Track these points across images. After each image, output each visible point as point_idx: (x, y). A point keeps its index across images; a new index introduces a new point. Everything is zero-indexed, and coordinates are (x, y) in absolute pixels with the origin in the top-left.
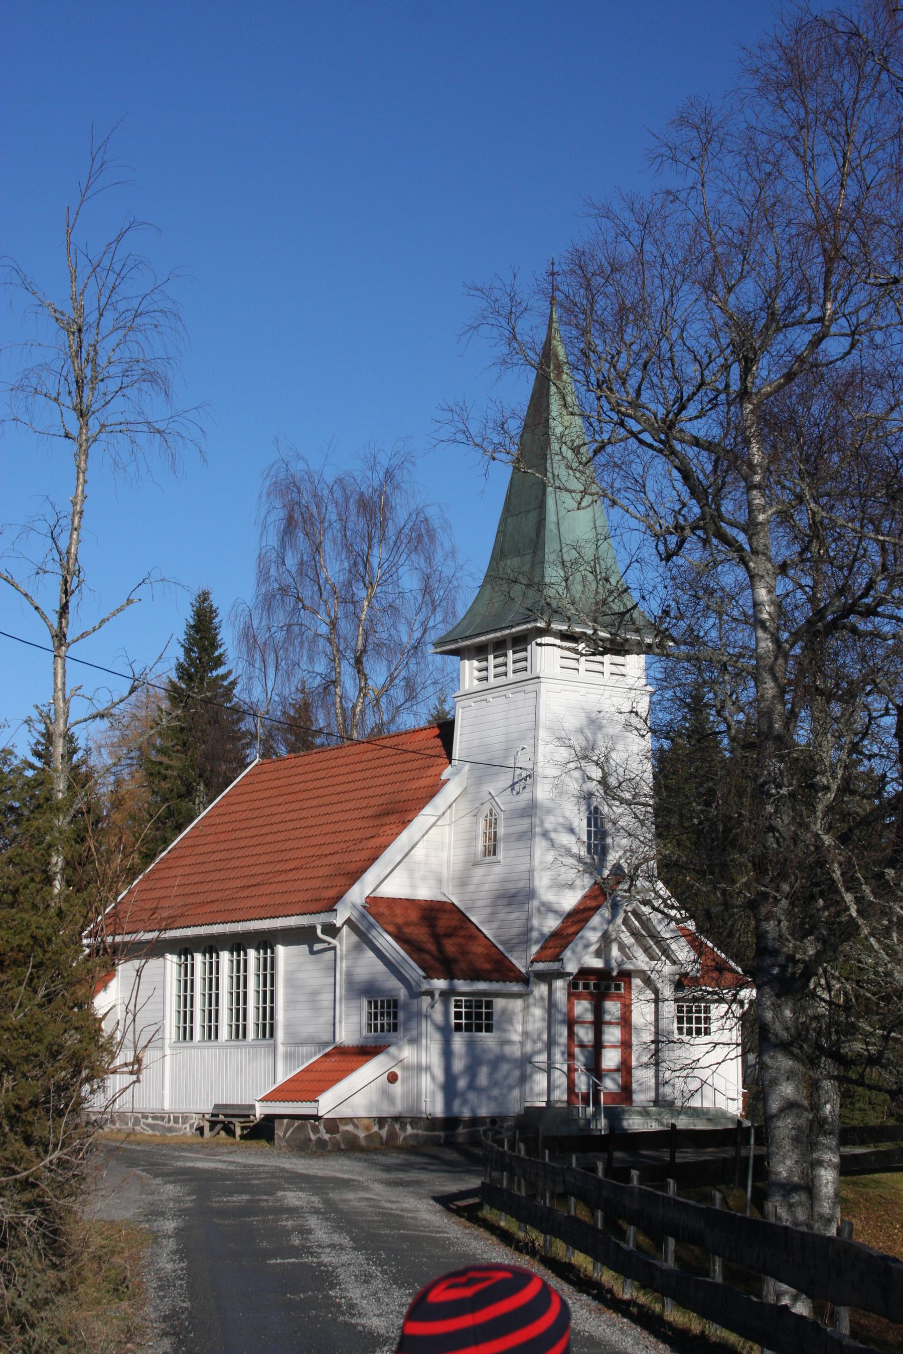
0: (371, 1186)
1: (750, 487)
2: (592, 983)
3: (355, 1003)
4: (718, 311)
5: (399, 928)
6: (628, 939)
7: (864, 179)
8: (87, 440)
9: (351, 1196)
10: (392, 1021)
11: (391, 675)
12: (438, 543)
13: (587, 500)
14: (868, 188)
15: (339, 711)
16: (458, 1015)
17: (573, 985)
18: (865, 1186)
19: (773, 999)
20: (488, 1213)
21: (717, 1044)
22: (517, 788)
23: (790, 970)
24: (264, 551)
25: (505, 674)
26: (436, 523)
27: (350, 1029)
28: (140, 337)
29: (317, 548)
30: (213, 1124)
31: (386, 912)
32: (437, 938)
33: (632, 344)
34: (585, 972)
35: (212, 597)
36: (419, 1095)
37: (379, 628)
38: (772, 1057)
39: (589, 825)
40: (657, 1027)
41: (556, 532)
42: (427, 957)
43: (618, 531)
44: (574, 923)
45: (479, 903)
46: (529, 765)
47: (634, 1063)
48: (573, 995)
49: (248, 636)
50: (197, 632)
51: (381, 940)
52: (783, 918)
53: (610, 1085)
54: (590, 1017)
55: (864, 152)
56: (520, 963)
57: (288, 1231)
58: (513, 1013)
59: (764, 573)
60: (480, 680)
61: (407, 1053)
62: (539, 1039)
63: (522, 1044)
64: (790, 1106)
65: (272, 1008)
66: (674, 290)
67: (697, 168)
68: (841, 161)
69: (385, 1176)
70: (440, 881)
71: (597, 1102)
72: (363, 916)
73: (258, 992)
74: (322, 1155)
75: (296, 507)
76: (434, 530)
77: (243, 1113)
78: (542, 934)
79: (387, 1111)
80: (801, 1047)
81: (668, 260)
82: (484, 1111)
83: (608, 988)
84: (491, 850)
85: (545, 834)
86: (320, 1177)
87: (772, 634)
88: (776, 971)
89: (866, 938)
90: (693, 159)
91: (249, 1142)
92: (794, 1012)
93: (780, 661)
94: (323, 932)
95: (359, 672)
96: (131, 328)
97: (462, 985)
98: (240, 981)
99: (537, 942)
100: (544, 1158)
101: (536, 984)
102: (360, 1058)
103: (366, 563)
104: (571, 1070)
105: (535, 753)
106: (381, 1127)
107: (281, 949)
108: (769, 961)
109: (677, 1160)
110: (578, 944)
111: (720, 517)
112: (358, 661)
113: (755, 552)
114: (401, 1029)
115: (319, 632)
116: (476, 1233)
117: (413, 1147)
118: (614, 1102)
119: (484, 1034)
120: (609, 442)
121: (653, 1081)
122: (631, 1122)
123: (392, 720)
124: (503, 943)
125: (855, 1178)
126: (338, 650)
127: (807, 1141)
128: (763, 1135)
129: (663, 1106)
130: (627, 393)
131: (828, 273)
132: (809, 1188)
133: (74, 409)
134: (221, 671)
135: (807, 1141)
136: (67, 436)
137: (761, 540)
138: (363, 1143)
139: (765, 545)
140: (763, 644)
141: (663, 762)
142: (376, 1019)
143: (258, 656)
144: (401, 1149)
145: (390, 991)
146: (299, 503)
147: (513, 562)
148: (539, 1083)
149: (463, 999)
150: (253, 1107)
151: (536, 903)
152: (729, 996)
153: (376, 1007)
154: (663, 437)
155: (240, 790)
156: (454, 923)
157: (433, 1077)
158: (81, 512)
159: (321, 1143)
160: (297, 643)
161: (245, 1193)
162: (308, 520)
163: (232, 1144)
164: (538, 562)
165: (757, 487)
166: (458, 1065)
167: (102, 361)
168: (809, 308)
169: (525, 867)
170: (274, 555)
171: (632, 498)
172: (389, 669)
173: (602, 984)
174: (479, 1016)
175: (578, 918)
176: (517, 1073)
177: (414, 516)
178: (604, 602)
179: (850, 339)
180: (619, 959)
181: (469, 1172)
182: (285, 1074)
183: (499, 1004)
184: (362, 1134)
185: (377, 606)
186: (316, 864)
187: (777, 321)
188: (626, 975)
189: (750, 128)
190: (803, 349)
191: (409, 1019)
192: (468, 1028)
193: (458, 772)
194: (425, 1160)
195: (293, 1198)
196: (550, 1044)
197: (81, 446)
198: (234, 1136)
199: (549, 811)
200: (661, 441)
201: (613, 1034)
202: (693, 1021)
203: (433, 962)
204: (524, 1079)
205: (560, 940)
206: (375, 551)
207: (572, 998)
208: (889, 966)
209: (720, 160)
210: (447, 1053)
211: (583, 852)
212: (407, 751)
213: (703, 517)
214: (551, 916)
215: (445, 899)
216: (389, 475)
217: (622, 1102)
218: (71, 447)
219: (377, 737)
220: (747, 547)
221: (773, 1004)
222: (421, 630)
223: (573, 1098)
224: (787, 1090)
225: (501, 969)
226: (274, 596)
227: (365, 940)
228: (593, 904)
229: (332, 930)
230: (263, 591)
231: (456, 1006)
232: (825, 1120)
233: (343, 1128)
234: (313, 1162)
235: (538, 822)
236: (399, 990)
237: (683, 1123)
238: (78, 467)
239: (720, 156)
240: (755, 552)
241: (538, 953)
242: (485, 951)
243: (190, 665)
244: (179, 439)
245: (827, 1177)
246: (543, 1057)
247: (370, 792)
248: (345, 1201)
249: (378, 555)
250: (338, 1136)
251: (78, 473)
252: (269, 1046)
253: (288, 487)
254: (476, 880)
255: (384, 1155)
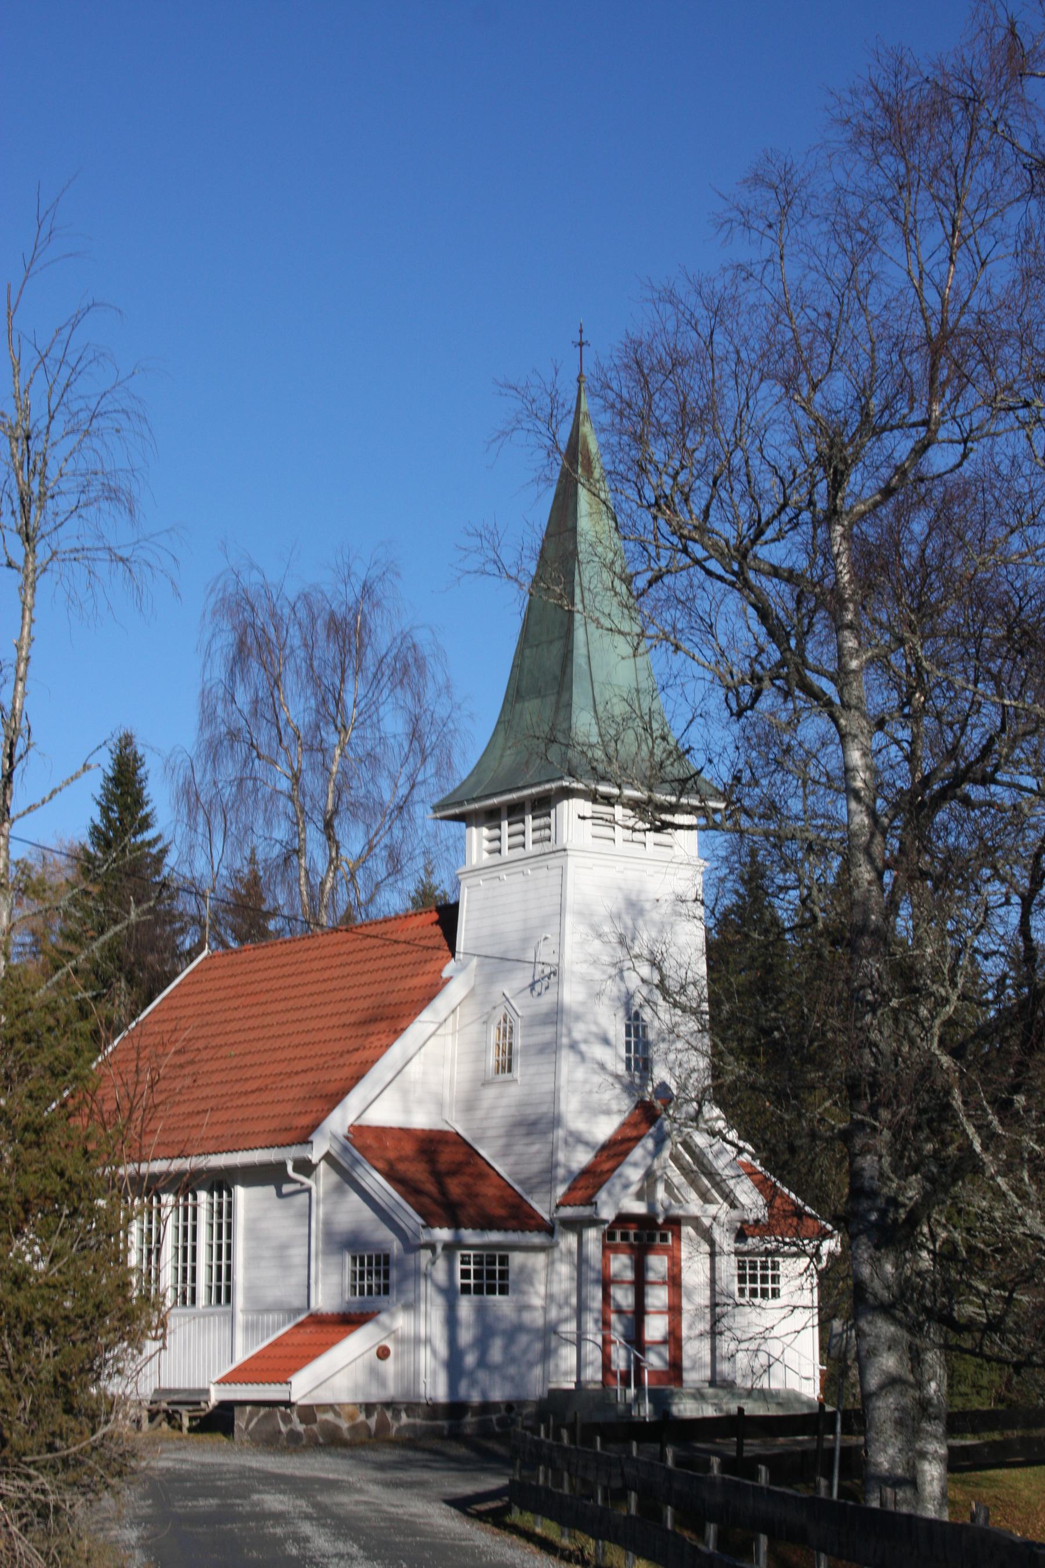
0: (366, 1487)
1: (840, 627)
2: (632, 1232)
3: (335, 1259)
4: (801, 412)
5: (391, 1164)
6: (676, 1176)
7: (978, 253)
8: (34, 571)
9: (343, 1499)
10: (382, 1281)
11: (370, 842)
12: (429, 675)
13: (645, 644)
14: (983, 264)
15: (303, 888)
16: (465, 1274)
17: (609, 1235)
18: (977, 1485)
19: (872, 1250)
20: (516, 1517)
21: (795, 1307)
22: (538, 987)
23: (891, 1216)
24: (208, 686)
25: (523, 845)
26: (426, 650)
27: (329, 1292)
28: (96, 443)
29: (276, 682)
30: (152, 1416)
31: (375, 1145)
32: (439, 1177)
33: (694, 451)
34: (623, 1219)
35: (136, 741)
36: (416, 1374)
37: (354, 783)
38: (870, 1323)
39: (628, 1034)
40: (713, 1290)
41: (586, 667)
42: (426, 1201)
43: (678, 681)
44: (609, 1158)
45: (490, 1133)
46: (554, 960)
47: (685, 1332)
48: (608, 1247)
49: (189, 796)
50: (117, 786)
51: (369, 1180)
52: (884, 1152)
53: (654, 1361)
54: (629, 1275)
55: (978, 218)
56: (542, 1207)
57: (280, 1539)
58: (534, 1271)
59: (858, 732)
60: (491, 852)
61: (402, 1322)
62: (567, 1302)
63: (545, 1309)
64: (892, 1382)
65: (229, 1267)
66: (750, 391)
67: (774, 236)
68: (950, 231)
69: (379, 1475)
70: (440, 1105)
71: (639, 1383)
72: (345, 1149)
73: (211, 1246)
74: (295, 1451)
75: (249, 630)
76: (424, 658)
77: (193, 1399)
78: (570, 1172)
79: (376, 1395)
80: (905, 1310)
81: (743, 355)
82: (497, 1395)
83: (652, 1238)
84: (506, 1066)
85: (573, 1046)
86: (301, 1478)
87: (868, 807)
88: (874, 1217)
89: (992, 1178)
90: (770, 226)
91: (200, 1437)
92: (896, 1266)
93: (878, 839)
94: (295, 1170)
95: (329, 838)
96: (87, 433)
97: (470, 1236)
98: (188, 1233)
99: (563, 1181)
100: (595, 1447)
101: (562, 1234)
102: (342, 1329)
103: (338, 701)
104: (607, 1342)
105: (560, 944)
106: (369, 1415)
107: (240, 1192)
108: (865, 1204)
109: (745, 1454)
110: (615, 1183)
111: (805, 663)
112: (328, 825)
113: (846, 706)
114: (393, 1292)
115: (278, 788)
116: (509, 1541)
117: (409, 1440)
118: (659, 1382)
119: (497, 1297)
120: (669, 572)
121: (707, 1358)
122: (682, 1407)
123: (371, 900)
124: (521, 1182)
125: (965, 1475)
126: (302, 811)
127: (910, 1423)
128: (857, 1419)
129: (722, 1387)
130: (690, 512)
131: (934, 367)
132: (912, 1482)
133: (19, 533)
134: (149, 835)
135: (910, 1423)
136: (10, 565)
137: (856, 690)
138: (347, 1435)
139: (859, 698)
140: (857, 819)
141: (716, 952)
142: (362, 1278)
143: (201, 818)
144: (394, 1443)
145: (380, 1243)
146: (253, 625)
147: (530, 707)
148: (566, 1358)
149: (472, 1253)
150: (207, 1391)
151: (561, 1133)
152: (810, 1249)
153: (362, 1264)
154: (736, 567)
155: (184, 990)
156: (460, 1157)
157: (434, 1352)
158: (28, 659)
159: (294, 1436)
160: (250, 801)
161: (213, 1497)
162: (264, 645)
163: (180, 1439)
164: (564, 706)
165: (850, 626)
166: (466, 1336)
167: (52, 472)
168: (911, 409)
169: (549, 1087)
170: (221, 692)
171: (696, 639)
172: (367, 833)
173: (645, 1234)
174: (491, 1274)
175: (615, 1150)
176: (538, 1346)
177: (399, 641)
178: (661, 765)
179: (960, 448)
180: (666, 1203)
181: (483, 1470)
182: (246, 1349)
183: (517, 1259)
184: (345, 1425)
185: (351, 755)
186: (284, 1084)
187: (872, 428)
188: (675, 1223)
189: (839, 188)
190: (904, 458)
191: (403, 1278)
192: (478, 1290)
193: (463, 968)
194: (426, 1456)
195: (274, 1501)
196: (581, 1309)
197: (27, 577)
198: (180, 1428)
199: (578, 1018)
200: (734, 573)
201: (658, 1297)
202: (758, 1280)
203: (435, 1208)
204: (547, 1354)
205: (591, 1180)
206: (349, 685)
207: (607, 1252)
208: (1020, 1210)
209: (802, 226)
210: (452, 1322)
211: (621, 1068)
212: (396, 942)
213: (782, 663)
214: (580, 1148)
215: (446, 1128)
216: (367, 590)
217: (669, 1382)
218: (16, 578)
219: (347, 923)
220: (837, 701)
221: (871, 1257)
222: (407, 787)
223: (610, 1378)
224: (889, 1362)
225: (517, 1215)
226: (221, 742)
227: (348, 1179)
228: (631, 1133)
229: (306, 1167)
230: (207, 735)
231: (463, 1263)
232: (929, 1402)
233: (321, 1417)
234: (285, 1459)
235: (564, 1031)
236: (392, 1242)
237: (753, 1408)
238: (24, 603)
239: (803, 222)
240: (846, 706)
241: (565, 1195)
242: (498, 1193)
243: (108, 828)
244: (145, 568)
245: (932, 1472)
246: (571, 1327)
247: (352, 993)
248: (338, 1505)
249: (353, 691)
250: (315, 1427)
251: (24, 610)
252: (225, 1314)
253: (238, 605)
254: (486, 1103)
255: (374, 1449)
